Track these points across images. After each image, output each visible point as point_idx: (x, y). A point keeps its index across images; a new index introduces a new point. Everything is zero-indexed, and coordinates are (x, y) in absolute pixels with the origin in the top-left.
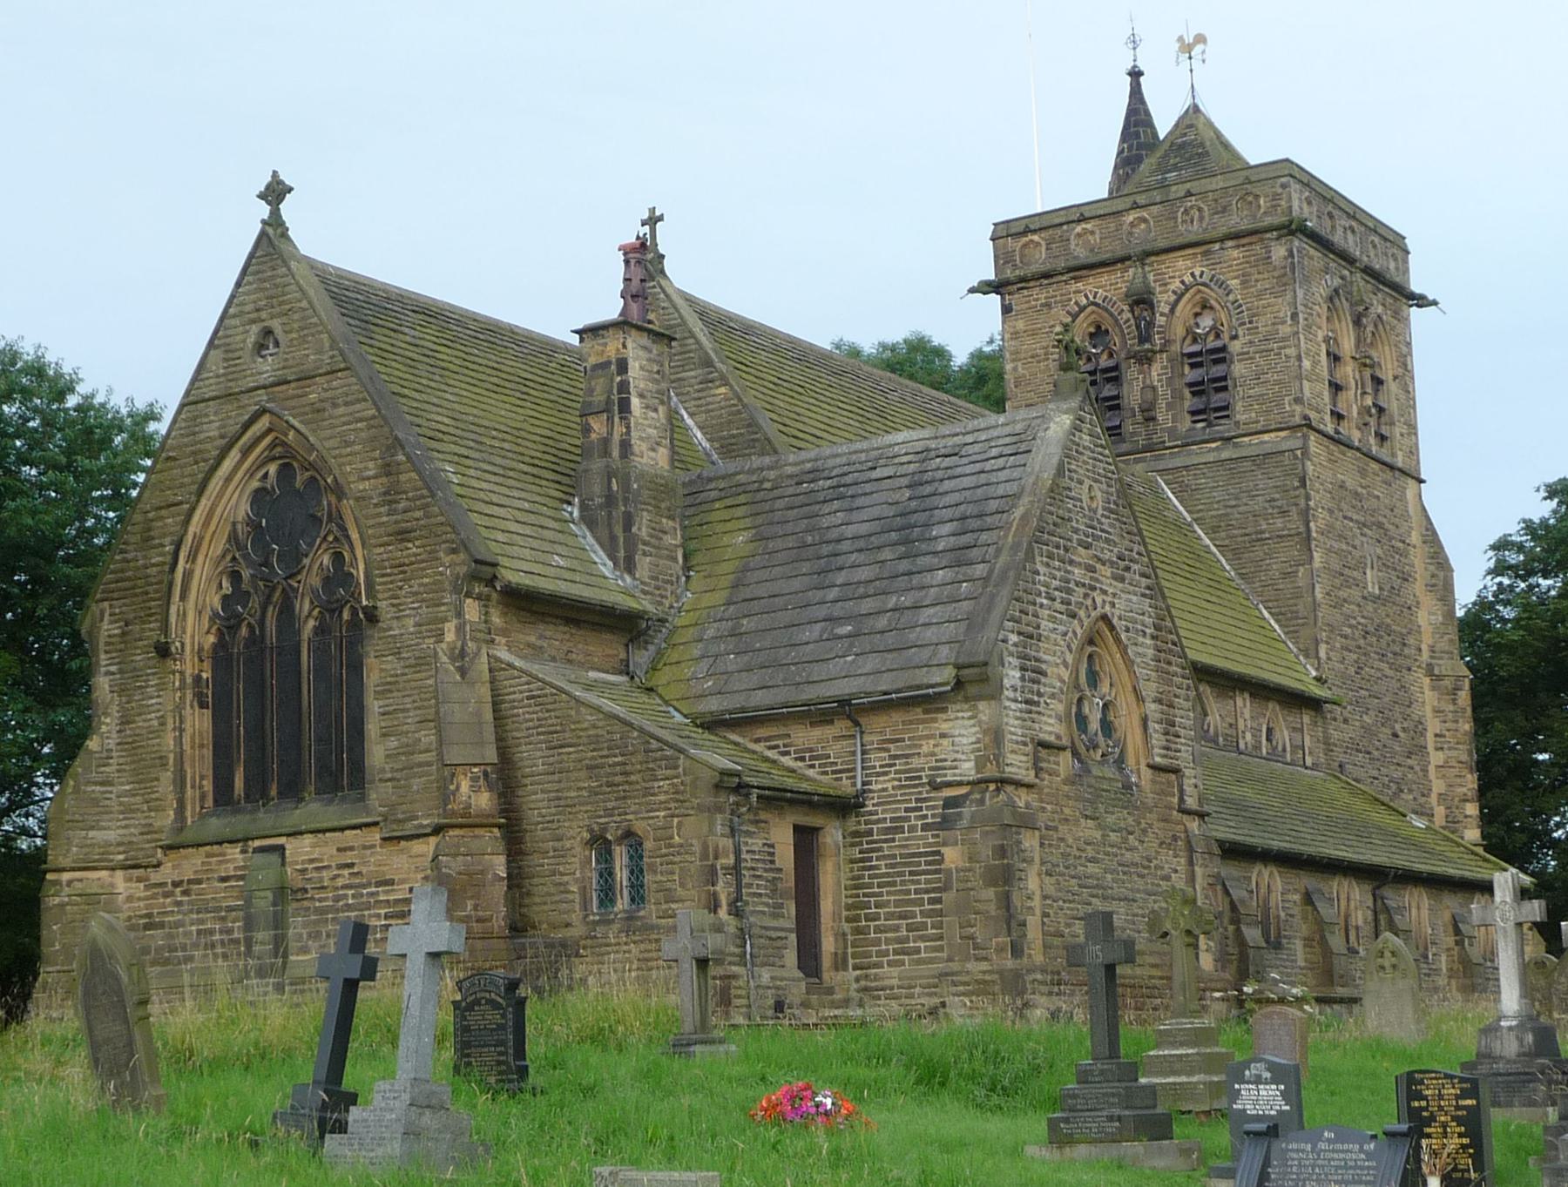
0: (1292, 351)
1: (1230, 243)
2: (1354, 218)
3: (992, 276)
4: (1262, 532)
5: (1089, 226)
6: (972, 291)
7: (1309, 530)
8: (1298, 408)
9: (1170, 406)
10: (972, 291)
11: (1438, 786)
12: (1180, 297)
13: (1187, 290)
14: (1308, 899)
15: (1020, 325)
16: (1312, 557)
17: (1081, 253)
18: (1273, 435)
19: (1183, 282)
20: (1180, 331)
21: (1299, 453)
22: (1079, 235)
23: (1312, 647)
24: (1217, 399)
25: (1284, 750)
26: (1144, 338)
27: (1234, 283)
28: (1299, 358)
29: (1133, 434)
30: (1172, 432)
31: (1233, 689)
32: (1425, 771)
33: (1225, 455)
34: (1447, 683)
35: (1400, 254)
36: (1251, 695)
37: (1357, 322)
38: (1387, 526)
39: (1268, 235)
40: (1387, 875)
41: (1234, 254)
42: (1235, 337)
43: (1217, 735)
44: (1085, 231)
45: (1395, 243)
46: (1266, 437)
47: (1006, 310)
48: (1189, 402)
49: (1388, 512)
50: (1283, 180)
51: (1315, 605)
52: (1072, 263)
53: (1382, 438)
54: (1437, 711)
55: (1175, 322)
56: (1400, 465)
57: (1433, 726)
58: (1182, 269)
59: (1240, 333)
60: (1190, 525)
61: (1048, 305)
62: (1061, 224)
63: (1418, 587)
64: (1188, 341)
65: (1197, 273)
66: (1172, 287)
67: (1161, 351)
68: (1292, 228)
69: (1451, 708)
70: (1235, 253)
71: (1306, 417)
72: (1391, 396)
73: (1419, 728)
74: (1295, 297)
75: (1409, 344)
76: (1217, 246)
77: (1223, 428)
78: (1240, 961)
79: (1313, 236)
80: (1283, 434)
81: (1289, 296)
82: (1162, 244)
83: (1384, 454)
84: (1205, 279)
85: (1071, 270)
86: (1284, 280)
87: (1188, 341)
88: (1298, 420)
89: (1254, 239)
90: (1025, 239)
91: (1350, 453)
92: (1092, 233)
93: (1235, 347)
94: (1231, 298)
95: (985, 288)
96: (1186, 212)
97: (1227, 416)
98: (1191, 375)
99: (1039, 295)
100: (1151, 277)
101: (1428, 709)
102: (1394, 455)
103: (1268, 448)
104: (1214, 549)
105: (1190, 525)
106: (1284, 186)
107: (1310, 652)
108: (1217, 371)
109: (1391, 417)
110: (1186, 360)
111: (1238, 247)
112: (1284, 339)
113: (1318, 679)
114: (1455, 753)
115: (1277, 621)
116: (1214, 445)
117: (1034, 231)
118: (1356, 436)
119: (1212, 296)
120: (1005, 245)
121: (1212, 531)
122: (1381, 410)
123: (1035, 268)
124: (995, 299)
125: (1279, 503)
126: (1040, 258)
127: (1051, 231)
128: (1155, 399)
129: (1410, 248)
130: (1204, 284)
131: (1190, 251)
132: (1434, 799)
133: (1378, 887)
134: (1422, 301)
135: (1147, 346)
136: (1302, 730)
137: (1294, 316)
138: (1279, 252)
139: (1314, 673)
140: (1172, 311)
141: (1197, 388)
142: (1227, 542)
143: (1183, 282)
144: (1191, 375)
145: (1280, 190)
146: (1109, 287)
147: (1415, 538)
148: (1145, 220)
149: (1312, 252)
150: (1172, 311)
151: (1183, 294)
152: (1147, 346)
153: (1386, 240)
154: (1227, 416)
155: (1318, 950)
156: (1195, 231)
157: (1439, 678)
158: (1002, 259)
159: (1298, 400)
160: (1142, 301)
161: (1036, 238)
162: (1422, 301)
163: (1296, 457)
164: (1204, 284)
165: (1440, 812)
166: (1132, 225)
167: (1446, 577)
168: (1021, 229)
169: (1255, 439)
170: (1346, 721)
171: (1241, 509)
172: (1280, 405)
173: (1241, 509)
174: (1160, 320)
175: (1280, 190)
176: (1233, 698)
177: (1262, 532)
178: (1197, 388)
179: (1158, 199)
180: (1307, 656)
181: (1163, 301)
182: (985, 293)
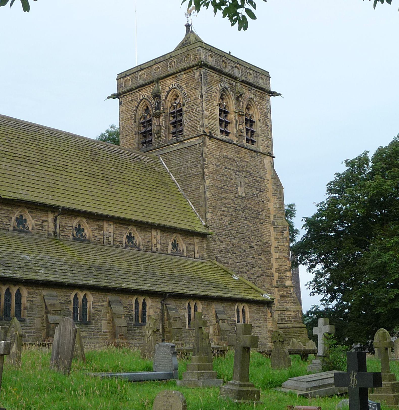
0: (200, 109)
1: (183, 73)
2: (238, 63)
3: (116, 92)
4: (190, 174)
5: (143, 72)
6: (109, 97)
7: (204, 172)
8: (202, 129)
9: (165, 132)
10: (109, 97)
11: (276, 266)
12: (168, 93)
13: (170, 91)
14: (109, 305)
15: (124, 108)
16: (205, 182)
17: (141, 82)
18: (194, 139)
19: (169, 88)
20: (169, 105)
21: (201, 144)
22: (140, 75)
23: (204, 214)
24: (180, 129)
25: (183, 252)
26: (158, 108)
27: (184, 87)
28: (203, 111)
29: (154, 143)
30: (165, 141)
31: (151, 229)
32: (269, 260)
33: (179, 147)
34: (280, 228)
35: (265, 78)
36: (161, 231)
37: (237, 99)
38: (251, 172)
39: (194, 68)
40: (166, 295)
41: (184, 76)
42: (184, 105)
43: (139, 245)
44: (143, 74)
45: (266, 75)
46: (192, 140)
47: (120, 103)
48: (172, 130)
49: (253, 167)
50: (198, 48)
51: (206, 199)
52: (138, 85)
53: (253, 142)
54: (276, 239)
55: (168, 103)
56: (261, 151)
57: (274, 244)
58: (169, 83)
59: (185, 104)
60: (169, 173)
61: (132, 101)
62: (135, 72)
63: (269, 194)
64: (172, 109)
65: (173, 84)
66: (166, 90)
67: (163, 113)
68: (202, 65)
69: (281, 237)
70: (184, 76)
71: (204, 131)
72: (258, 127)
73: (268, 245)
74: (202, 89)
75: (269, 109)
76: (179, 74)
77: (180, 139)
78: (47, 329)
79: (211, 68)
80: (197, 138)
81: (200, 90)
82: (163, 75)
83: (253, 147)
84: (176, 86)
85: (138, 87)
86: (198, 83)
87: (172, 109)
88: (202, 133)
89: (190, 70)
90: (126, 79)
91: (231, 146)
92: (144, 74)
93: (184, 109)
94: (183, 92)
95: (114, 96)
96: (170, 63)
97: (182, 134)
98: (172, 120)
99: (129, 97)
100: (160, 87)
101: (272, 238)
102: (258, 147)
103: (192, 144)
104: (176, 181)
105: (169, 173)
106: (198, 50)
107: (204, 216)
108: (180, 118)
109: (258, 134)
110: (171, 115)
111: (185, 74)
112: (198, 105)
113: (206, 226)
114: (282, 254)
115: (194, 206)
116: (177, 144)
117: (128, 76)
118: (235, 140)
119: (178, 91)
120: (120, 81)
121: (175, 175)
122: (253, 132)
123: (128, 88)
124: (117, 100)
125: (194, 163)
126: (130, 85)
127: (133, 75)
128: (160, 130)
129: (270, 76)
130: (175, 88)
131: (171, 77)
132: (274, 270)
133: (164, 300)
134: (274, 94)
135: (158, 111)
136: (194, 245)
137: (202, 96)
138: (197, 74)
139: (204, 224)
140: (166, 99)
141: (174, 124)
142: (179, 178)
143: (169, 88)
144: (172, 120)
145: (197, 52)
146: (147, 92)
147: (268, 177)
148: (159, 68)
149: (212, 74)
150: (166, 99)
151: (169, 92)
152: (158, 111)
153: (257, 72)
154: (182, 134)
155: (111, 325)
156: (172, 70)
157: (277, 227)
158: (119, 86)
159: (201, 126)
160: (157, 96)
161: (129, 78)
162: (274, 94)
163: (200, 146)
164: (175, 88)
165: (276, 275)
166: (155, 70)
167: (280, 190)
168: (124, 76)
169: (189, 141)
170: (221, 241)
171: (184, 166)
172: (197, 128)
173: (184, 166)
174: (163, 102)
175: (197, 52)
176: (151, 232)
177: (190, 174)
178: (174, 124)
179: (162, 60)
180: (202, 218)
181: (163, 95)
182: (114, 98)
